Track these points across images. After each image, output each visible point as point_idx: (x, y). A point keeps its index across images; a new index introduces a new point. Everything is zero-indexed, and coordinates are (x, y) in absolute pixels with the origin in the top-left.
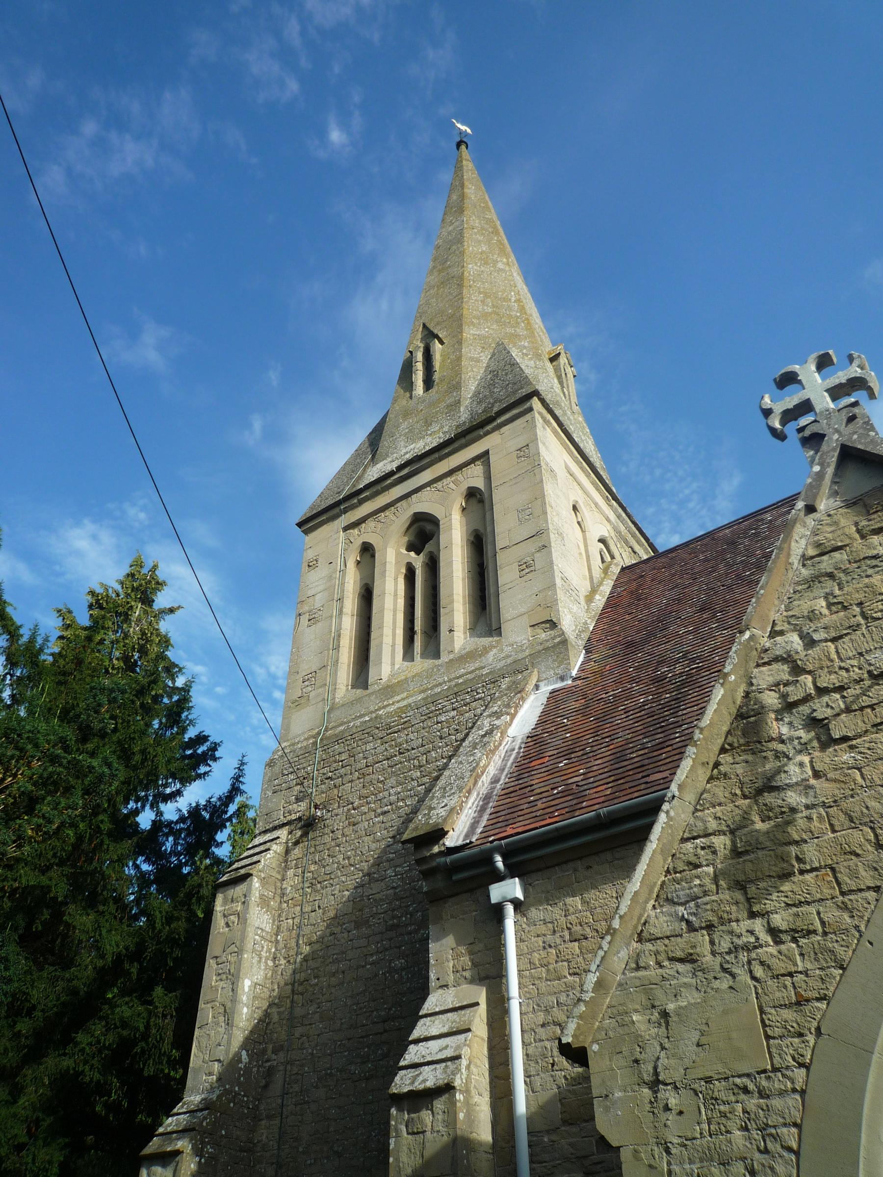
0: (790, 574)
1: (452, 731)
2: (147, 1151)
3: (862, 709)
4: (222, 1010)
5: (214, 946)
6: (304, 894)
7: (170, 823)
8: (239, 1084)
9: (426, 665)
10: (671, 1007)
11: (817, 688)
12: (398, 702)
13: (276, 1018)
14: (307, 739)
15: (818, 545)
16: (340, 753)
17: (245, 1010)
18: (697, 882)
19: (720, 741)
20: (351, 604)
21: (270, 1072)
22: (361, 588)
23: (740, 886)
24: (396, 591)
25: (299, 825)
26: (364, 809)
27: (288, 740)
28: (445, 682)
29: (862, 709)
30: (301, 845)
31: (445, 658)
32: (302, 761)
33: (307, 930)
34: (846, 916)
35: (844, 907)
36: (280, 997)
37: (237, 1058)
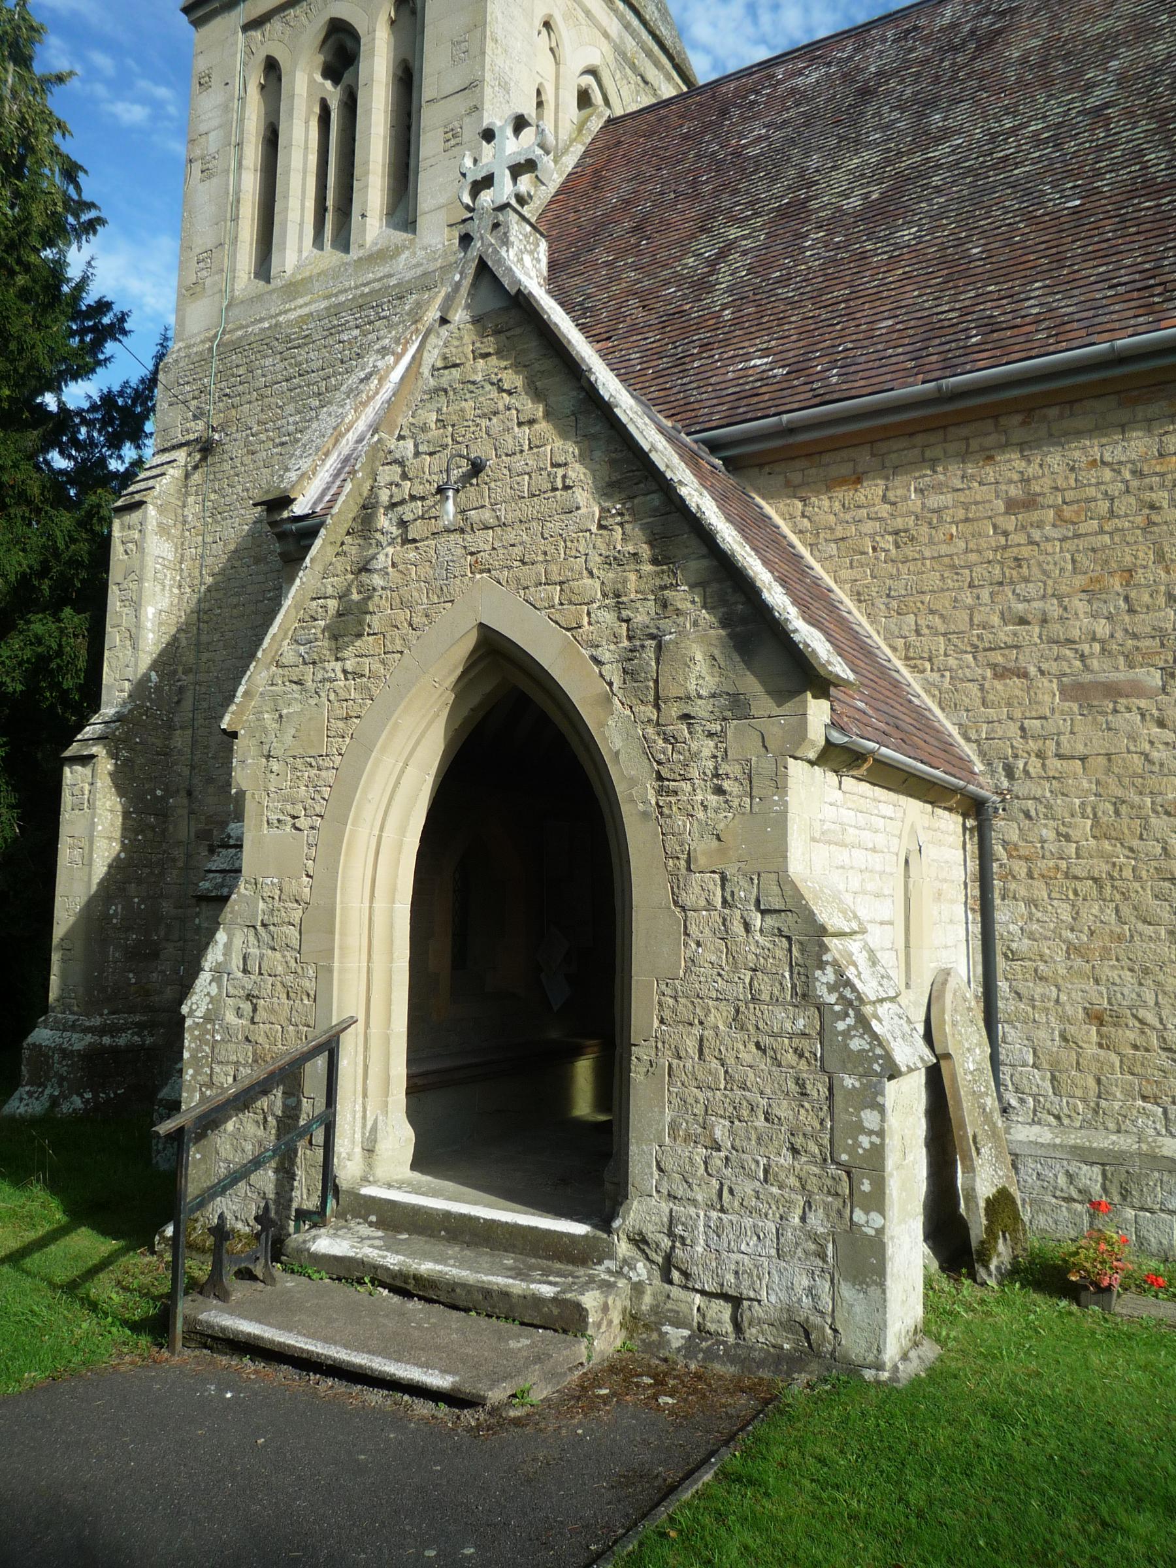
0: (420, 383)
1: (353, 356)
2: (68, 753)
3: (430, 518)
4: (127, 635)
5: (116, 573)
6: (205, 524)
7: (79, 412)
8: (151, 700)
9: (334, 258)
10: (285, 712)
11: (410, 495)
12: (301, 307)
13: (184, 642)
14: (203, 342)
15: (445, 358)
16: (237, 366)
17: (151, 635)
18: (313, 631)
19: (346, 526)
20: (253, 154)
21: (181, 690)
22: (265, 129)
23: (335, 637)
24: (306, 141)
25: (198, 447)
26: (263, 437)
27: (183, 340)
28: (350, 289)
29: (430, 518)
30: (200, 470)
31: (355, 253)
32: (198, 370)
33: (209, 561)
34: (382, 667)
35: (383, 662)
36: (187, 624)
37: (146, 677)
